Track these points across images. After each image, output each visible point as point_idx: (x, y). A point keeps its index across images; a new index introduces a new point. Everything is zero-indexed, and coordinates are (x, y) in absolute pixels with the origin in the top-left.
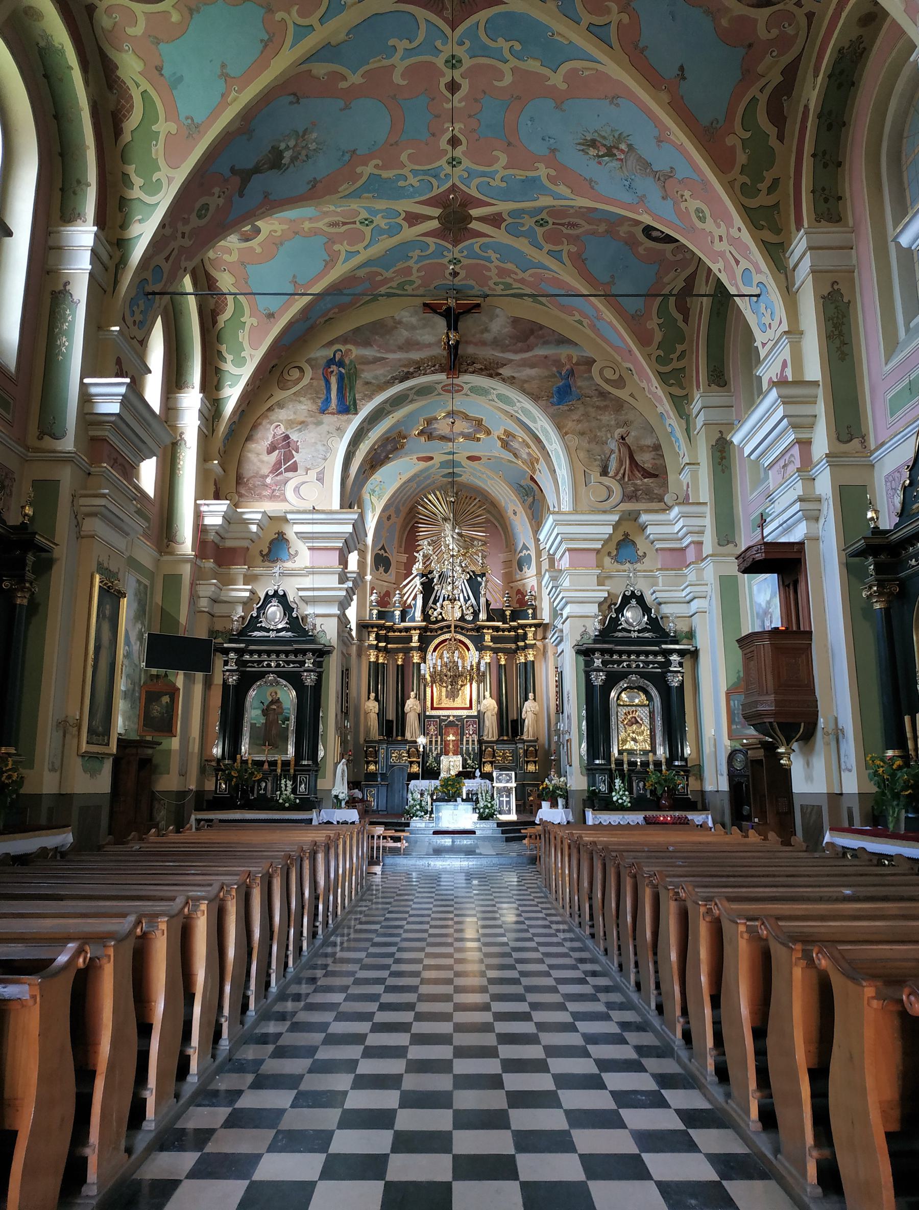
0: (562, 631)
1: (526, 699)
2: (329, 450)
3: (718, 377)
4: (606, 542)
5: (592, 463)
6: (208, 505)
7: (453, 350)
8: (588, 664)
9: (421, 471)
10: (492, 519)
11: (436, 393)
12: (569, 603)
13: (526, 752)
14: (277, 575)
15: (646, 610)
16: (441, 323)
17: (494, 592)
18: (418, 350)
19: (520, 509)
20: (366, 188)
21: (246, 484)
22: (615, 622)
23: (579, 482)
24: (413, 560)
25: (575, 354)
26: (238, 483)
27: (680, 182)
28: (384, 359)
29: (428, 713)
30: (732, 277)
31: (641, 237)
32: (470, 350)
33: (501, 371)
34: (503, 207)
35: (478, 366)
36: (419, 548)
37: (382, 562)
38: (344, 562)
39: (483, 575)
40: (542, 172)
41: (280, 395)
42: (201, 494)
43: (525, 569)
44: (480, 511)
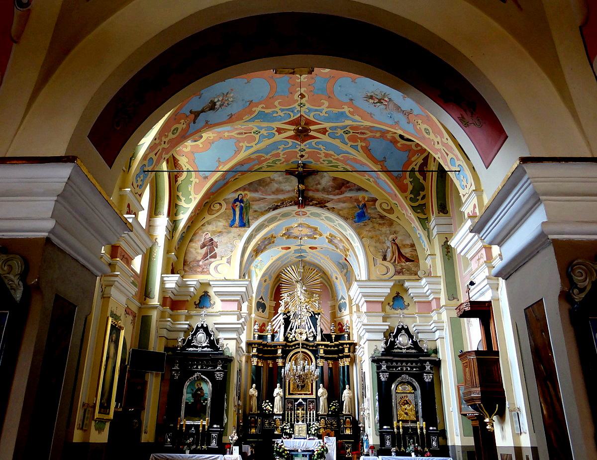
0: (363, 348)
1: (344, 389)
2: (234, 246)
3: (443, 209)
4: (387, 297)
5: (378, 254)
7: (301, 193)
8: (379, 368)
9: (284, 255)
10: (325, 282)
11: (292, 216)
12: (366, 337)
13: (345, 422)
14: (203, 315)
15: (410, 336)
16: (295, 180)
17: (325, 325)
19: (339, 277)
20: (256, 117)
21: (189, 265)
22: (393, 343)
23: (371, 264)
25: (367, 196)
26: (184, 264)
27: (416, 116)
28: (265, 198)
29: (286, 397)
30: (445, 161)
31: (399, 139)
32: (311, 194)
33: (327, 204)
34: (327, 125)
35: (315, 202)
36: (283, 298)
37: (261, 306)
38: (240, 308)
39: (319, 314)
40: (346, 109)
41: (209, 218)
42: (165, 271)
43: (343, 311)
44: (317, 277)
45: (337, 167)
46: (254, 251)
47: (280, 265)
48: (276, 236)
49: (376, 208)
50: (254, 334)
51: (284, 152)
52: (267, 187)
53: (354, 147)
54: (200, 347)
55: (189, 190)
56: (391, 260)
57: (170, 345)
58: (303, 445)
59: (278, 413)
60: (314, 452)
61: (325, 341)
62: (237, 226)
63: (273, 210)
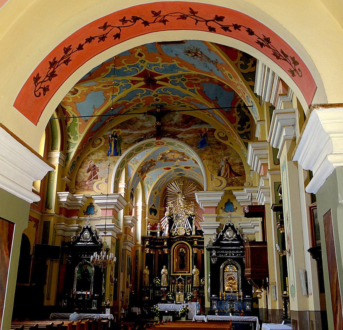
6: (61, 194)
7: (158, 127)
14: (88, 220)
15: (235, 231)
16: (154, 119)
18: (146, 129)
21: (79, 185)
22: (222, 236)
24: (165, 211)
25: (207, 127)
26: (76, 185)
32: (166, 128)
33: (177, 136)
35: (169, 134)
36: (168, 205)
41: (92, 150)
42: (59, 190)
45: (185, 106)
46: (139, 172)
47: (166, 181)
48: (156, 160)
49: (214, 137)
50: (148, 231)
51: (143, 97)
52: (134, 125)
53: (193, 91)
54: (86, 242)
55: (76, 130)
56: (224, 176)
57: (67, 241)
58: (172, 308)
59: (164, 286)
60: (179, 312)
61: (198, 235)
62: (113, 155)
63: (138, 142)
